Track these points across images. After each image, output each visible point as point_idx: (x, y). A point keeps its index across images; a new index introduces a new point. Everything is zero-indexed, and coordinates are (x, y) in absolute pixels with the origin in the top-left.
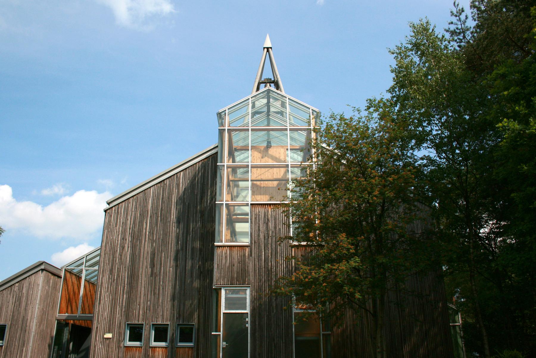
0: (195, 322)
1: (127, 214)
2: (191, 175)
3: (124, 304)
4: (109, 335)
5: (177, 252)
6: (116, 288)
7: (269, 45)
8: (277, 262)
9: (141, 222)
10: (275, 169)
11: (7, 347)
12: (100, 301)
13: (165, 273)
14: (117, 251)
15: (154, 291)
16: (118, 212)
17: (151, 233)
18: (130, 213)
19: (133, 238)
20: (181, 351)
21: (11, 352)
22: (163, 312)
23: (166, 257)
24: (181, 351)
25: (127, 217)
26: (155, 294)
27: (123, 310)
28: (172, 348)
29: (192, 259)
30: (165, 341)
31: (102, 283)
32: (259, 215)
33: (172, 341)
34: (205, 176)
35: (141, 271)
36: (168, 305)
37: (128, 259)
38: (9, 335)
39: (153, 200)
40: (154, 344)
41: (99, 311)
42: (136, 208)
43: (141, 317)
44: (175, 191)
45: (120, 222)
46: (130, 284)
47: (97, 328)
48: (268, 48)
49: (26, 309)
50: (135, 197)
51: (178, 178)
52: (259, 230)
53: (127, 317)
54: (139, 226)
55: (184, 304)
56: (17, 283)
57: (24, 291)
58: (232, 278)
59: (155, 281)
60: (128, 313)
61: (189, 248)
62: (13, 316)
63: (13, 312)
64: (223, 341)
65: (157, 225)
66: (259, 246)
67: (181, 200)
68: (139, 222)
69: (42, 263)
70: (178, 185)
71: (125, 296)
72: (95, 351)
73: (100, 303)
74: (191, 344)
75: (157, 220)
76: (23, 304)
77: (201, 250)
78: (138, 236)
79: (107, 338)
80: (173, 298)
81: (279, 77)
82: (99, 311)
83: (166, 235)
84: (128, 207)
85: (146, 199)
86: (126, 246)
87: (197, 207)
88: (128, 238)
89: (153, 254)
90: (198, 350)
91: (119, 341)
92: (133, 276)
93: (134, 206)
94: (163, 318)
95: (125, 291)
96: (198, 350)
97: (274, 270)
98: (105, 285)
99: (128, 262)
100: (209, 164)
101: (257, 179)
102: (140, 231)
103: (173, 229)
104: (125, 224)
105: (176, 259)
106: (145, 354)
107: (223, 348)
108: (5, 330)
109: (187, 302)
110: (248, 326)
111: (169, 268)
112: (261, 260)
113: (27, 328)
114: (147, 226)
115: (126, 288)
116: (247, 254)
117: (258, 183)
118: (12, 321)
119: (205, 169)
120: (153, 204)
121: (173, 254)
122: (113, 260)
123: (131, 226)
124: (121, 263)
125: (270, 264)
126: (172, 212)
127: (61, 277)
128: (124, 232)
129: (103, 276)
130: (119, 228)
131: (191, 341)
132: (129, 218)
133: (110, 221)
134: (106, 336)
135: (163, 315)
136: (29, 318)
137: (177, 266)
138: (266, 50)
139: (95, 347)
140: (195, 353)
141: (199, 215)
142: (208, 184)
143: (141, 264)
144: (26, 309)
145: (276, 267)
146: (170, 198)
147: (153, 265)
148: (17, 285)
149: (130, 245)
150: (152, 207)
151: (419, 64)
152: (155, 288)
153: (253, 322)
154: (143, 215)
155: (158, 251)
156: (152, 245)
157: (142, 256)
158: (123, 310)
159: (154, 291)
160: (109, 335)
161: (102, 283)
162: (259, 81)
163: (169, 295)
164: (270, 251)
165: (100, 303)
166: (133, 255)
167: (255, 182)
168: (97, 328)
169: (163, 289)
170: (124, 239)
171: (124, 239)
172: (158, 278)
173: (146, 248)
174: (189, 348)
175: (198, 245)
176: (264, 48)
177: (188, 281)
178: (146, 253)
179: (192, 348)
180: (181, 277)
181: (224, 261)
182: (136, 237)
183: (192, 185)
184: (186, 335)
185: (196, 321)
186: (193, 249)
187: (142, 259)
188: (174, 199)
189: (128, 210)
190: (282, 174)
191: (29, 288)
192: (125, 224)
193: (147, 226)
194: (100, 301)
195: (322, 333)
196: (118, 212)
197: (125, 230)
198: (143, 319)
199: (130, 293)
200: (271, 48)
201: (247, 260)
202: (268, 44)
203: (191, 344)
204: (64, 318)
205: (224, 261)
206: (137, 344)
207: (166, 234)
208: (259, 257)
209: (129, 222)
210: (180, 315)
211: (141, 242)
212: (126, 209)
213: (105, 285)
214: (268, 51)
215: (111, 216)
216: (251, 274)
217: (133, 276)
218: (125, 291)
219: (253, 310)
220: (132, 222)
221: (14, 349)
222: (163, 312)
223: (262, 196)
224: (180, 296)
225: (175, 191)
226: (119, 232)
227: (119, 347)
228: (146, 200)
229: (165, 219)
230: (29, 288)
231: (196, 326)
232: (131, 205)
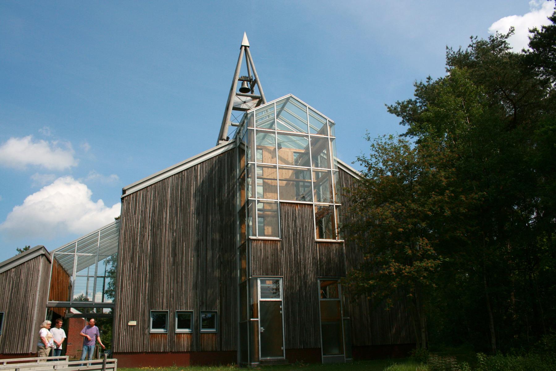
0: (218, 310)
1: (146, 202)
2: (208, 168)
3: (147, 292)
4: (133, 323)
5: (198, 242)
6: (138, 276)
7: (247, 44)
8: (304, 257)
9: (161, 211)
10: (284, 170)
11: (5, 336)
12: (122, 289)
13: (187, 262)
14: (137, 239)
15: (177, 280)
16: (136, 200)
17: (172, 222)
18: (148, 201)
19: (153, 227)
20: (206, 336)
21: (10, 341)
22: (186, 299)
23: (188, 247)
24: (206, 336)
25: (146, 205)
26: (177, 282)
27: (147, 298)
28: (197, 334)
29: (213, 249)
30: (164, 328)
31: (123, 271)
32: (288, 213)
33: (197, 328)
34: (226, 173)
35: (162, 259)
36: (190, 294)
37: (149, 247)
38: (7, 323)
39: (172, 190)
40: (178, 331)
41: (121, 299)
42: (155, 196)
43: (165, 304)
44: (194, 183)
45: (139, 210)
46: (152, 272)
47: (120, 315)
48: (245, 47)
49: (25, 296)
50: (153, 186)
51: (196, 171)
52: (288, 226)
53: (151, 305)
54: (159, 215)
55: (207, 292)
56: (13, 268)
57: (23, 277)
58: (267, 270)
59: (177, 270)
60: (151, 302)
61: (209, 239)
62: (10, 302)
63: (11, 300)
64: (261, 326)
65: (177, 215)
66: (289, 241)
67: (200, 191)
68: (159, 211)
69: (43, 248)
70: (196, 177)
71: (147, 284)
72: (119, 338)
73: (122, 291)
74: (214, 330)
75: (177, 210)
76: (22, 291)
77: (220, 242)
78: (158, 225)
79: (131, 326)
80: (195, 286)
81: (257, 76)
82: (121, 299)
83: (187, 225)
84: (146, 195)
85: (165, 189)
86: (147, 234)
87: (215, 200)
88: (149, 227)
89: (174, 243)
90: (221, 335)
91: (144, 329)
92: (155, 266)
93: (152, 195)
94: (187, 306)
95: (148, 279)
96: (221, 335)
97: (302, 262)
98: (127, 273)
99: (149, 250)
100: (224, 159)
101: (268, 177)
102: (160, 220)
103: (193, 220)
104: (144, 212)
105: (197, 249)
106: (171, 340)
107: (261, 333)
108: (2, 318)
109: (209, 291)
110: (282, 312)
111: (190, 257)
112: (291, 253)
113: (29, 316)
114: (167, 215)
115: (148, 276)
116: (279, 248)
117: (269, 181)
118: (9, 309)
119: (221, 165)
120: (172, 194)
121: (193, 244)
122: (133, 248)
123: (151, 215)
124: (142, 251)
125: (299, 257)
126: (192, 203)
127: (50, 263)
128: (144, 221)
129: (124, 264)
130: (138, 217)
131: (212, 327)
132: (148, 206)
133: (128, 209)
134: (129, 324)
135: (186, 303)
136: (30, 306)
137: (198, 256)
138: (243, 48)
139: (119, 334)
140: (219, 339)
141: (217, 208)
142: (224, 179)
143: (163, 253)
144: (25, 296)
145: (305, 260)
146: (188, 189)
147: (174, 255)
148: (13, 270)
149: (150, 234)
150: (171, 197)
151: (450, 110)
152: (178, 277)
153: (287, 309)
154: (162, 205)
155: (179, 240)
156: (173, 235)
157: (163, 246)
158: (147, 298)
159: (177, 280)
160: (133, 323)
161: (123, 271)
162: (258, 84)
163: (192, 284)
164: (298, 246)
165: (122, 291)
166: (154, 244)
167: (266, 181)
168: (120, 315)
169: (186, 277)
170: (143, 227)
171: (143, 227)
172: (180, 267)
173: (167, 236)
174: (212, 333)
175: (217, 236)
176: (242, 46)
177: (210, 270)
178: (167, 242)
179: (215, 333)
180: (202, 267)
181: (259, 254)
182: (156, 226)
183: (210, 178)
184: (209, 323)
185: (218, 307)
186: (213, 240)
187: (163, 248)
188: (193, 190)
189: (146, 197)
190: (290, 175)
191: (28, 274)
192: (144, 212)
193: (167, 215)
194: (122, 289)
195: (343, 318)
196: (136, 200)
197: (145, 218)
198: (167, 307)
199: (152, 281)
200: (249, 47)
201: (279, 253)
202: (246, 42)
203: (214, 330)
204: (54, 305)
205: (259, 254)
206: (161, 331)
207: (186, 224)
208: (290, 250)
209: (148, 210)
210: (203, 303)
211: (161, 231)
212: (145, 197)
213: (127, 273)
214: (246, 50)
215: (129, 203)
216: (284, 266)
217: (155, 266)
218: (148, 279)
219: (286, 298)
220: (151, 211)
221: (14, 338)
222: (186, 299)
223: (273, 194)
224: (202, 284)
225: (194, 183)
226: (138, 220)
227: (144, 334)
228: (164, 189)
229: (184, 209)
230: (28, 274)
231: (219, 313)
232: (150, 195)
